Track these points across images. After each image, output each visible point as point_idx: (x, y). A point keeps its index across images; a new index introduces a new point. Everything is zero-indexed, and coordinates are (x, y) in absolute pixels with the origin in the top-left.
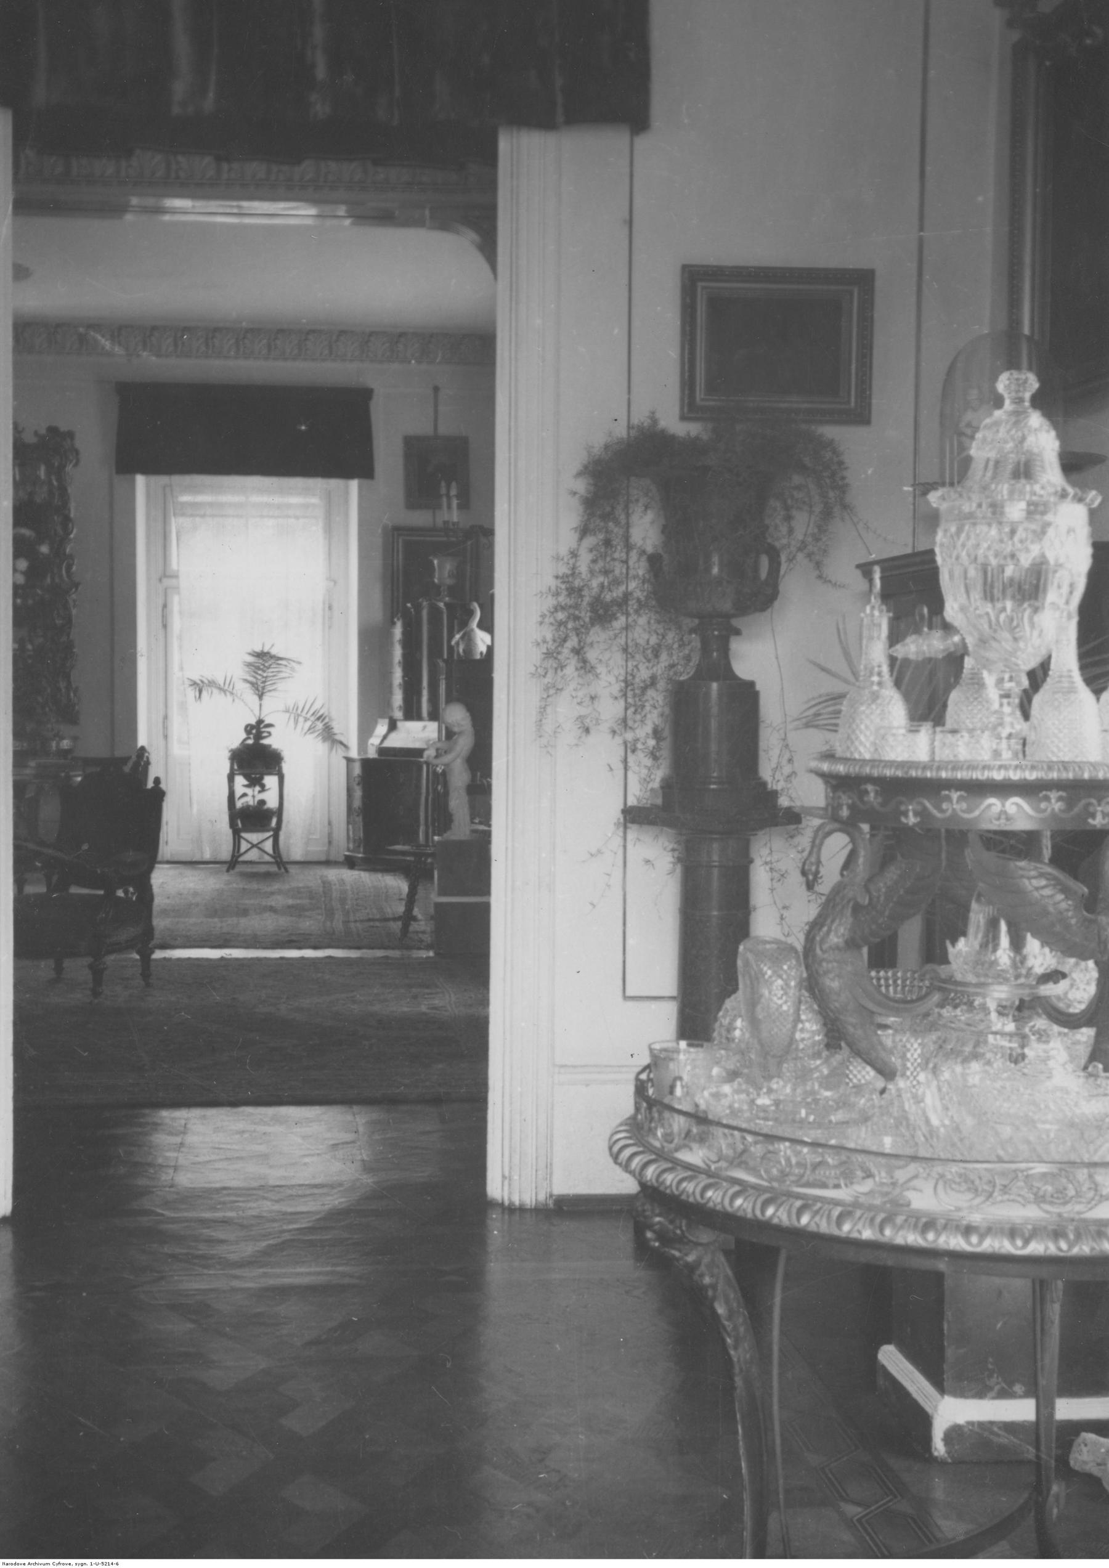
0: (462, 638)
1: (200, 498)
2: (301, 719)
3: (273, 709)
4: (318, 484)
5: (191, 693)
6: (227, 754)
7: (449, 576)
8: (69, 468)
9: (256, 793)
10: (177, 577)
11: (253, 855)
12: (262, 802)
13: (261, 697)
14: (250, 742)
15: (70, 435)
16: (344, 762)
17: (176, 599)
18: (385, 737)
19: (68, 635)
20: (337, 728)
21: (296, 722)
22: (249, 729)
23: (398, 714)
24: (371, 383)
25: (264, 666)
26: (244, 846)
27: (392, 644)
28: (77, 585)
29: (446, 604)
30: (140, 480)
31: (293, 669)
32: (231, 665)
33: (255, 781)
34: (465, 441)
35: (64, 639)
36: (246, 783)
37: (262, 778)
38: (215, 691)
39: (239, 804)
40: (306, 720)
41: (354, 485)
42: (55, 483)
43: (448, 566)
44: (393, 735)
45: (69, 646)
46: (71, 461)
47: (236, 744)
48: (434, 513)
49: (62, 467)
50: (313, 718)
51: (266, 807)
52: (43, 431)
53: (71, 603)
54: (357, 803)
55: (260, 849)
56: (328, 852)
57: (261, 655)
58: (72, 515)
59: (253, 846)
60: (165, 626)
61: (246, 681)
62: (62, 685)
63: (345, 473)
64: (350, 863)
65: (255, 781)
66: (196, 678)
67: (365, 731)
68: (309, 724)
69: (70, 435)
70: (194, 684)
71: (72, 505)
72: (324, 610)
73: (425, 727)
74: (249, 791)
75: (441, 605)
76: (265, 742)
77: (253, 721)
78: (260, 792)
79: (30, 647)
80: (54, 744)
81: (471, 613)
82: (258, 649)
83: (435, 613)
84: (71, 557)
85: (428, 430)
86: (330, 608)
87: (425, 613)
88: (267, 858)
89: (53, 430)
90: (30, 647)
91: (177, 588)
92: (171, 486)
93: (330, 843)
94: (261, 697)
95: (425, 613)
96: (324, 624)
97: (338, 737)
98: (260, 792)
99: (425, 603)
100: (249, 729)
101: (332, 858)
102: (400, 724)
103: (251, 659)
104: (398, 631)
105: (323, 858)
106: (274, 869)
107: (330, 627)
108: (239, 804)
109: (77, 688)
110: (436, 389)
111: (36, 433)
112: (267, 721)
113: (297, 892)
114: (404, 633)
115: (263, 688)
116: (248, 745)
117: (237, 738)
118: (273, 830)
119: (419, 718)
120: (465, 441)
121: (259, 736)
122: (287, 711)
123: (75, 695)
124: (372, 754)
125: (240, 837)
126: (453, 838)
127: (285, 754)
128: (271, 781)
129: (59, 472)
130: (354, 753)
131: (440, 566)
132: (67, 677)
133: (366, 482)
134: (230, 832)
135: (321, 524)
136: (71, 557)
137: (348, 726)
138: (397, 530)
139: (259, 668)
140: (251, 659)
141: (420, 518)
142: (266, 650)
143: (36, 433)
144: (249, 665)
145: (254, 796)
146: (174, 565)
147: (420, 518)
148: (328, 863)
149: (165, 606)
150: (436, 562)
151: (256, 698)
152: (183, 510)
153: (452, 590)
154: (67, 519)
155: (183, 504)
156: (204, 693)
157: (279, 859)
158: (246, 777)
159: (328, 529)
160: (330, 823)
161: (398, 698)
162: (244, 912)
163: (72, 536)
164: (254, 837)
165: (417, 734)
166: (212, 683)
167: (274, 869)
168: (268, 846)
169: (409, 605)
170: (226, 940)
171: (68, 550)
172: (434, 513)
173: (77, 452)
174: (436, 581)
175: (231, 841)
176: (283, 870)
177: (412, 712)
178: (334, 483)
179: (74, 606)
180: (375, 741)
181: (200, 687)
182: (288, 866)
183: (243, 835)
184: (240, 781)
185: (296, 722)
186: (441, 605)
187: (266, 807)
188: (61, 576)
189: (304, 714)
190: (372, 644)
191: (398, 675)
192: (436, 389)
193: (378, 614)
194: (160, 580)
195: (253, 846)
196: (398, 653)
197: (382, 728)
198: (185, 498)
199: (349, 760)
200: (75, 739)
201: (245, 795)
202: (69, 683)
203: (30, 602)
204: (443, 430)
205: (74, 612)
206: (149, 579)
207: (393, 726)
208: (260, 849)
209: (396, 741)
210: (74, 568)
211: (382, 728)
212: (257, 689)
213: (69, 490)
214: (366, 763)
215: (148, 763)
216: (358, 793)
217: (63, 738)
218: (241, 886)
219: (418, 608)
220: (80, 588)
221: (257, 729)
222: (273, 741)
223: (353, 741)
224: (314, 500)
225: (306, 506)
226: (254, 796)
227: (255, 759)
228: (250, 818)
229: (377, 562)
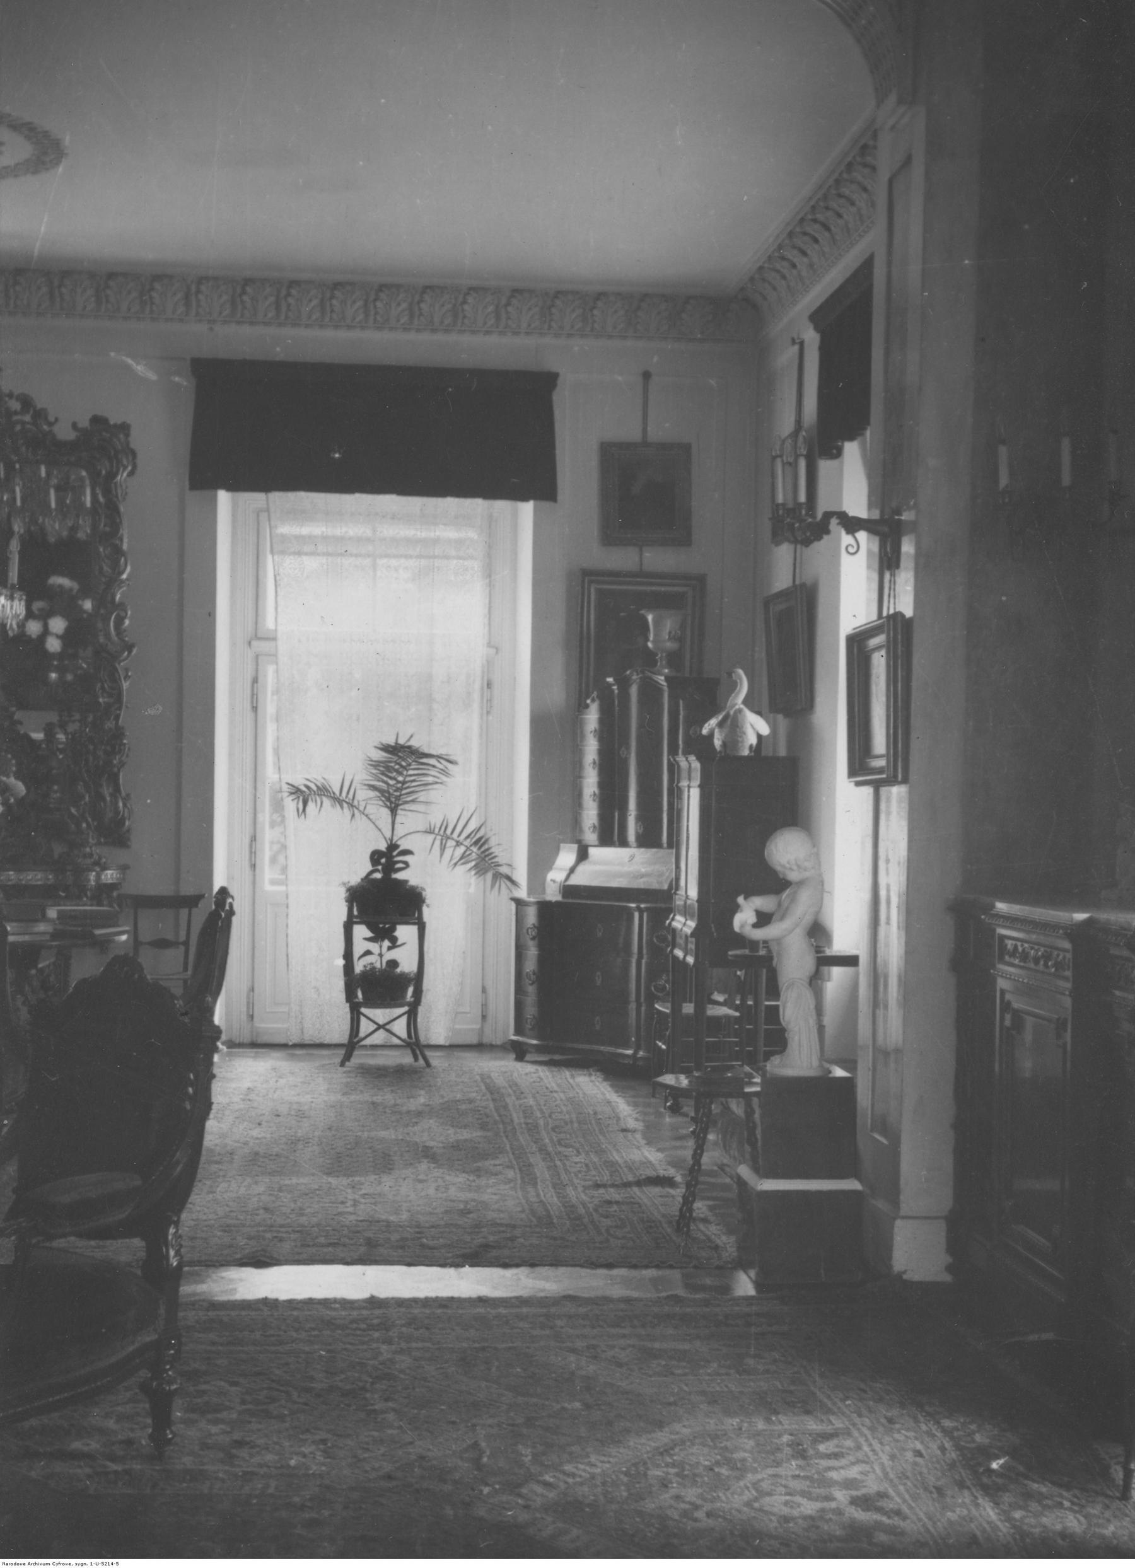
0: (721, 725)
1: (305, 530)
2: (451, 843)
3: (410, 827)
4: (477, 505)
5: (291, 805)
6: (342, 893)
7: (670, 639)
8: (122, 477)
9: (385, 949)
10: (274, 639)
11: (379, 1037)
12: (393, 964)
13: (394, 811)
14: (378, 876)
15: (125, 428)
16: (513, 905)
17: (271, 670)
18: (572, 870)
19: (117, 717)
20: (501, 855)
21: (443, 849)
22: (376, 857)
23: (591, 837)
24: (551, 363)
25: (401, 768)
26: (365, 1027)
27: (583, 736)
28: (130, 648)
29: (667, 679)
30: (223, 497)
31: (445, 772)
32: (347, 761)
33: (383, 933)
34: (686, 448)
35: (109, 725)
36: (369, 934)
37: (394, 929)
38: (327, 802)
39: (359, 968)
40: (458, 844)
41: (527, 508)
42: (101, 499)
43: (669, 625)
44: (581, 868)
45: (118, 734)
46: (125, 468)
47: (355, 879)
48: (641, 550)
49: (112, 475)
50: (468, 843)
51: (398, 970)
52: (84, 423)
53: (122, 674)
54: (530, 966)
55: (388, 1031)
56: (481, 1031)
57: (394, 750)
58: (125, 547)
59: (380, 1027)
60: (255, 709)
61: (373, 788)
62: (106, 791)
63: (518, 494)
64: (520, 1052)
65: (383, 933)
66: (299, 782)
67: (540, 862)
68: (462, 849)
69: (125, 428)
70: (296, 791)
71: (125, 532)
72: (482, 688)
73: (632, 857)
74: (374, 947)
75: (661, 679)
76: (400, 876)
77: (383, 846)
78: (389, 948)
79: (61, 737)
80: (92, 876)
81: (733, 686)
82: (391, 741)
83: (650, 693)
84: (122, 606)
85: (635, 435)
86: (489, 685)
87: (634, 690)
88: (396, 1041)
89: (98, 421)
90: (61, 737)
91: (274, 656)
92: (268, 510)
93: (484, 1017)
94: (394, 811)
95: (634, 690)
96: (482, 708)
97: (504, 870)
98: (389, 948)
99: (634, 677)
100: (376, 857)
101: (485, 1040)
102: (593, 852)
103: (380, 755)
104: (592, 718)
105: (474, 1040)
106: (407, 1059)
107: (488, 713)
108: (359, 968)
109: (128, 795)
110: (647, 376)
111: (74, 426)
112: (404, 845)
113: (451, 1113)
114: (601, 721)
115: (398, 798)
116: (375, 880)
117: (359, 869)
118: (409, 1004)
119: (623, 843)
120: (686, 448)
121: (390, 868)
122: (430, 831)
123: (125, 805)
124: (553, 895)
125: (360, 1013)
126: (789, 1072)
127: (428, 894)
128: (406, 933)
129: (106, 483)
130: (522, 893)
131: (656, 622)
132: (114, 779)
133: (546, 505)
134: (346, 1008)
135: (476, 565)
136: (122, 606)
137: (515, 849)
138: (588, 575)
139: (389, 769)
140: (380, 755)
141: (622, 559)
142: (401, 741)
143: (74, 426)
144: (376, 764)
145: (381, 955)
146: (270, 624)
147: (622, 559)
148: (480, 1047)
149: (255, 680)
150: (650, 618)
151: (385, 813)
152: (283, 546)
153: (674, 659)
154: (118, 551)
155: (284, 538)
156: (311, 806)
157: (414, 1044)
158: (370, 927)
159: (489, 573)
160: (484, 990)
161: (590, 814)
162: (384, 1163)
163: (124, 576)
164: (380, 1015)
165: (614, 865)
166: (323, 791)
167: (407, 1059)
168: (400, 1027)
169: (610, 680)
170: (371, 1243)
171: (118, 597)
172: (641, 550)
173: (134, 454)
174: (650, 645)
175: (349, 1016)
176: (421, 1062)
177: (611, 834)
178: (501, 506)
179: (127, 677)
180: (556, 876)
181: (303, 795)
182: (428, 1053)
183: (363, 1010)
184: (361, 932)
185: (443, 849)
186: (661, 679)
187: (398, 970)
188: (107, 635)
189: (455, 835)
190: (552, 737)
191: (591, 782)
192: (647, 376)
193: (557, 696)
194: (250, 643)
195: (380, 1027)
196: (591, 749)
197: (566, 857)
198: (284, 529)
199: (519, 902)
200: (124, 868)
201: (368, 953)
202: (117, 789)
203: (69, 677)
204: (656, 434)
205: (125, 685)
206: (233, 644)
207: (583, 855)
208: (388, 1031)
209: (584, 877)
210: (127, 622)
211: (566, 857)
212: (388, 799)
213: (122, 509)
214: (545, 908)
215: (231, 913)
216: (532, 952)
217: (104, 868)
218: (366, 1097)
219: (624, 684)
220: (135, 651)
221: (387, 858)
222: (411, 876)
223: (521, 874)
224: (472, 534)
225: (459, 542)
226: (381, 955)
227: (384, 900)
228: (376, 987)
229: (558, 625)
